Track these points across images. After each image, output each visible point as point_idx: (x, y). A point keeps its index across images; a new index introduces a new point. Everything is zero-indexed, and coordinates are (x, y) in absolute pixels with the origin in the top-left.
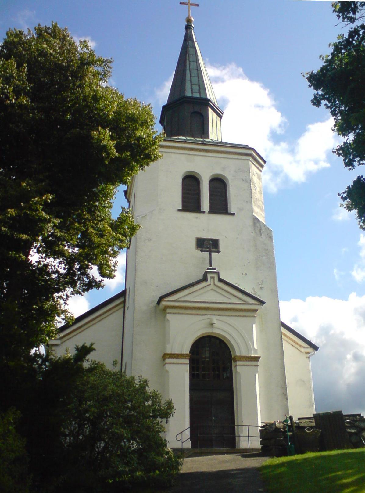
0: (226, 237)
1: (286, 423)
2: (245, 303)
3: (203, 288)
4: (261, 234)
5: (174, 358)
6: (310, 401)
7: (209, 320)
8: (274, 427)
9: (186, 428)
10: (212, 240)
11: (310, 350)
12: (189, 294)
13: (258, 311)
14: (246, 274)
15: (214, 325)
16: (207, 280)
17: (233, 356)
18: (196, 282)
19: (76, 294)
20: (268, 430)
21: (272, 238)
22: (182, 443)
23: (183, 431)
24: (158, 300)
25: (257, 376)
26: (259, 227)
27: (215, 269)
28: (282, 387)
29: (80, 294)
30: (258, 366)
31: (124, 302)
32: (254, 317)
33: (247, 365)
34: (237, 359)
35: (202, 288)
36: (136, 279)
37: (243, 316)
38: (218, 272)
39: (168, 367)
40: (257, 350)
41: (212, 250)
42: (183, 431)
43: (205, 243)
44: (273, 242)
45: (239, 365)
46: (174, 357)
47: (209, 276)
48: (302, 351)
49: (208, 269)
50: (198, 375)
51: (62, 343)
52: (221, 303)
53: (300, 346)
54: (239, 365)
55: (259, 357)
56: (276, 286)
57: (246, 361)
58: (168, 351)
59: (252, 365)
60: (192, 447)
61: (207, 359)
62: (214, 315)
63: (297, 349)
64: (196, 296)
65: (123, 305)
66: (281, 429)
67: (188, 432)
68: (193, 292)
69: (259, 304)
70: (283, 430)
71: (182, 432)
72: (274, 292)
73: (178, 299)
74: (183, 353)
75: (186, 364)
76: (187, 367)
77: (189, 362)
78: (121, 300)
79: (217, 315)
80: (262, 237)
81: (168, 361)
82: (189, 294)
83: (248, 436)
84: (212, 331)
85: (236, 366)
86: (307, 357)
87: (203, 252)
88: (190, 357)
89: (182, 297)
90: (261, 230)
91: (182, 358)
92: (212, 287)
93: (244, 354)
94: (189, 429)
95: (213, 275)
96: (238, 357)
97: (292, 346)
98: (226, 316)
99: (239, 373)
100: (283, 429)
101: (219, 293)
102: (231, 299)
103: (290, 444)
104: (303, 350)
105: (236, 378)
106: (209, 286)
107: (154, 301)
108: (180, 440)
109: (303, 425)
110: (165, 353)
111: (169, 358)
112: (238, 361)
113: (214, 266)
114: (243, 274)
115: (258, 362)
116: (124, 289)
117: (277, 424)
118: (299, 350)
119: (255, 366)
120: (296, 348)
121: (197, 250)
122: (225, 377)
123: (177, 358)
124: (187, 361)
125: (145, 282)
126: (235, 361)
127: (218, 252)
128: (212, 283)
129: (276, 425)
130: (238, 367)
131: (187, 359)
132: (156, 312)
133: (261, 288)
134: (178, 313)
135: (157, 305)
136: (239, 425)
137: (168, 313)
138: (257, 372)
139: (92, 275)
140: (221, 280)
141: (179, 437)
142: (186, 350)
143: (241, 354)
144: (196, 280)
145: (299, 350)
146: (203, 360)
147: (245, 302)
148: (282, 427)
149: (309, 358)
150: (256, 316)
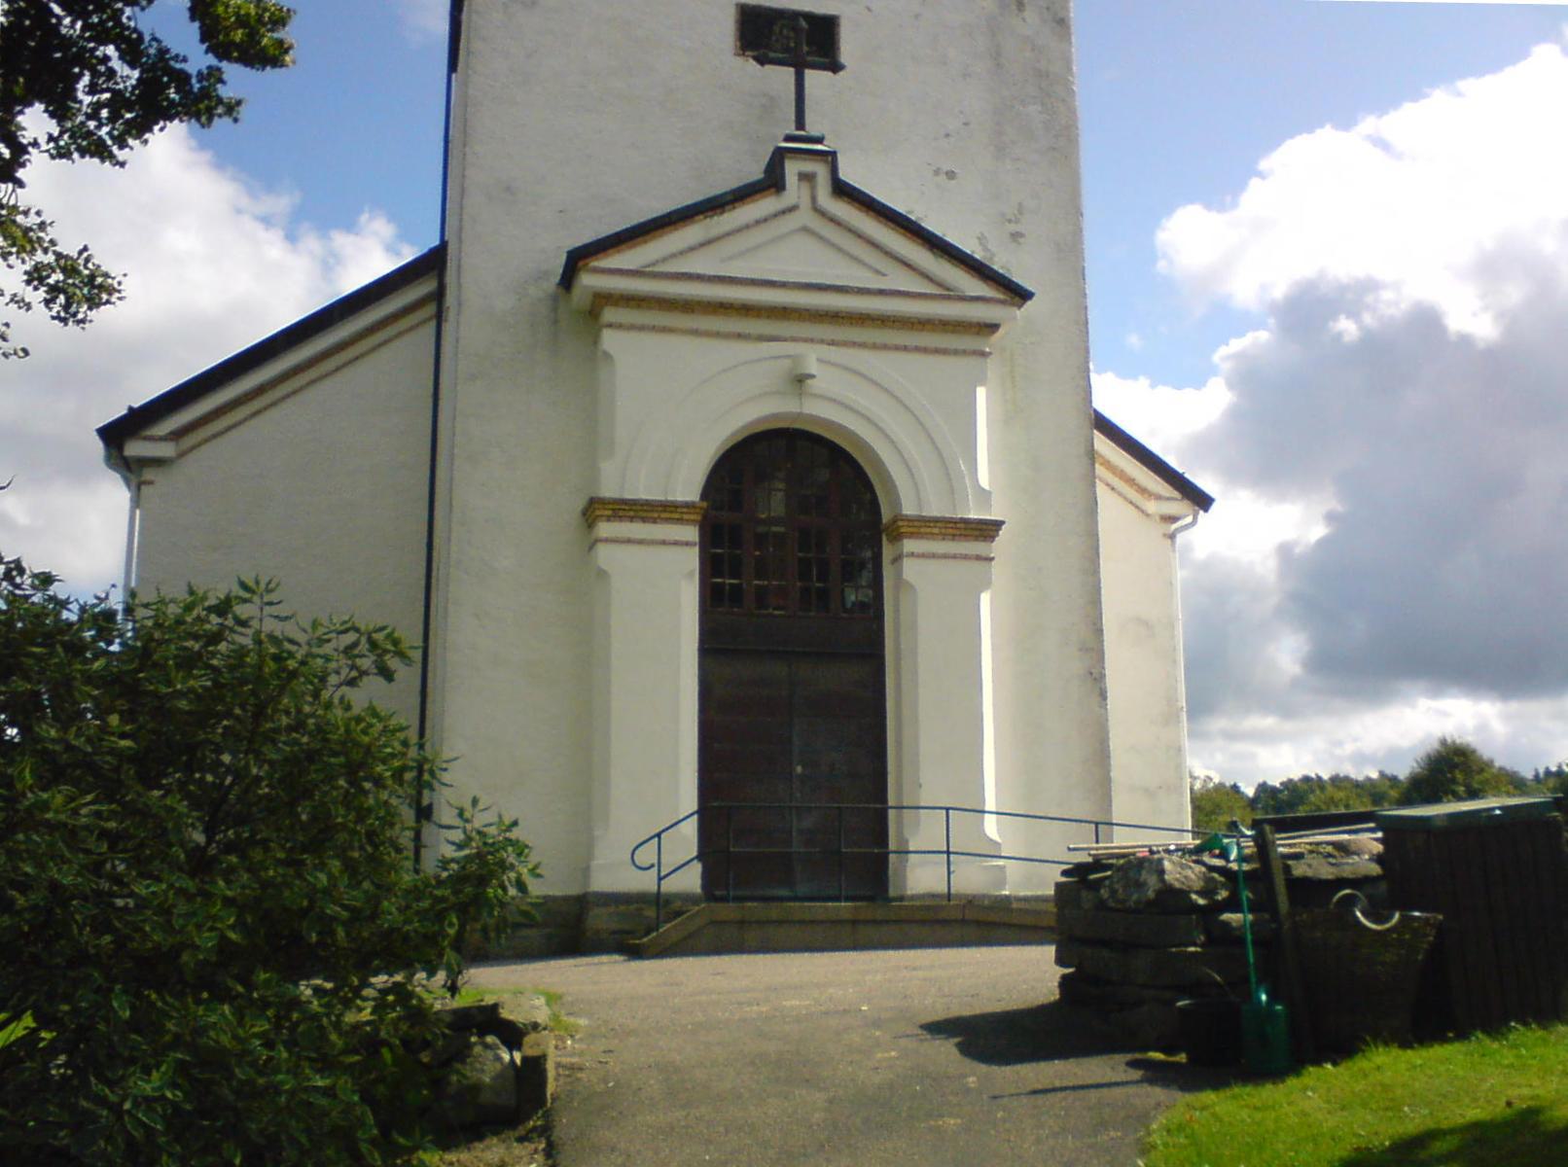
0: (869, 9)
1: (1218, 862)
2: (946, 293)
3: (765, 220)
5: (632, 519)
6: (1171, 701)
7: (787, 362)
8: (1152, 882)
9: (681, 817)
10: (809, 17)
11: (1180, 507)
12: (702, 245)
13: (1001, 331)
14: (951, 175)
15: (809, 382)
17: (886, 516)
18: (733, 192)
19: (83, 153)
20: (1113, 892)
21: (1068, 28)
22: (660, 879)
23: (663, 831)
24: (564, 272)
25: (985, 598)
27: (819, 140)
28: (1084, 649)
29: (100, 151)
30: (992, 559)
31: (439, 295)
32: (983, 354)
33: (945, 556)
35: (758, 222)
36: (467, 173)
37: (937, 351)
38: (833, 154)
39: (605, 555)
40: (990, 493)
41: (809, 58)
42: (663, 831)
43: (776, 29)
44: (1071, 43)
46: (632, 513)
47: (792, 168)
48: (1150, 512)
49: (789, 138)
50: (737, 591)
51: (182, 455)
53: (1143, 491)
54: (912, 555)
55: (998, 524)
56: (1078, 232)
57: (944, 537)
58: (609, 490)
59: (966, 557)
60: (704, 886)
61: (774, 529)
62: (812, 341)
63: (1131, 503)
64: (741, 254)
65: (430, 309)
66: (1194, 897)
67: (690, 829)
70: (1201, 901)
71: (658, 835)
72: (1070, 254)
73: (664, 260)
74: (670, 498)
76: (691, 559)
77: (697, 539)
78: (424, 287)
79: (822, 341)
80: (1024, 20)
81: (605, 529)
82: (702, 245)
83: (948, 853)
84: (799, 411)
85: (898, 559)
86: (1165, 535)
87: (769, 68)
88: (705, 517)
89: (673, 256)
91: (668, 520)
92: (805, 217)
93: (934, 509)
94: (696, 817)
95: (808, 166)
96: (910, 520)
97: (1110, 491)
98: (863, 345)
100: (1201, 893)
101: (833, 245)
102: (884, 275)
103: (1264, 997)
104: (1152, 507)
105: (897, 611)
106: (788, 216)
107: (545, 275)
108: (652, 866)
109: (1310, 873)
110: (594, 495)
111: (609, 519)
112: (911, 535)
113: (812, 128)
114: (937, 172)
115: (994, 544)
116: (436, 242)
117: (1167, 865)
118: (1137, 507)
119: (978, 558)
120: (1126, 499)
121: (740, 60)
122: (849, 605)
123: (644, 520)
124: (691, 533)
125: (508, 189)
126: (897, 537)
127: (835, 67)
129: (1162, 872)
130: (907, 563)
131: (688, 522)
132: (556, 322)
133: (1016, 236)
134: (654, 329)
135: (561, 291)
136: (905, 804)
137: (610, 326)
138: (986, 584)
139: (154, 39)
140: (843, 190)
141: (647, 855)
142: (688, 487)
143: (920, 506)
144: (734, 184)
145: (1137, 507)
146: (761, 529)
147: (948, 289)
148: (1198, 885)
149: (1172, 537)
150: (990, 353)
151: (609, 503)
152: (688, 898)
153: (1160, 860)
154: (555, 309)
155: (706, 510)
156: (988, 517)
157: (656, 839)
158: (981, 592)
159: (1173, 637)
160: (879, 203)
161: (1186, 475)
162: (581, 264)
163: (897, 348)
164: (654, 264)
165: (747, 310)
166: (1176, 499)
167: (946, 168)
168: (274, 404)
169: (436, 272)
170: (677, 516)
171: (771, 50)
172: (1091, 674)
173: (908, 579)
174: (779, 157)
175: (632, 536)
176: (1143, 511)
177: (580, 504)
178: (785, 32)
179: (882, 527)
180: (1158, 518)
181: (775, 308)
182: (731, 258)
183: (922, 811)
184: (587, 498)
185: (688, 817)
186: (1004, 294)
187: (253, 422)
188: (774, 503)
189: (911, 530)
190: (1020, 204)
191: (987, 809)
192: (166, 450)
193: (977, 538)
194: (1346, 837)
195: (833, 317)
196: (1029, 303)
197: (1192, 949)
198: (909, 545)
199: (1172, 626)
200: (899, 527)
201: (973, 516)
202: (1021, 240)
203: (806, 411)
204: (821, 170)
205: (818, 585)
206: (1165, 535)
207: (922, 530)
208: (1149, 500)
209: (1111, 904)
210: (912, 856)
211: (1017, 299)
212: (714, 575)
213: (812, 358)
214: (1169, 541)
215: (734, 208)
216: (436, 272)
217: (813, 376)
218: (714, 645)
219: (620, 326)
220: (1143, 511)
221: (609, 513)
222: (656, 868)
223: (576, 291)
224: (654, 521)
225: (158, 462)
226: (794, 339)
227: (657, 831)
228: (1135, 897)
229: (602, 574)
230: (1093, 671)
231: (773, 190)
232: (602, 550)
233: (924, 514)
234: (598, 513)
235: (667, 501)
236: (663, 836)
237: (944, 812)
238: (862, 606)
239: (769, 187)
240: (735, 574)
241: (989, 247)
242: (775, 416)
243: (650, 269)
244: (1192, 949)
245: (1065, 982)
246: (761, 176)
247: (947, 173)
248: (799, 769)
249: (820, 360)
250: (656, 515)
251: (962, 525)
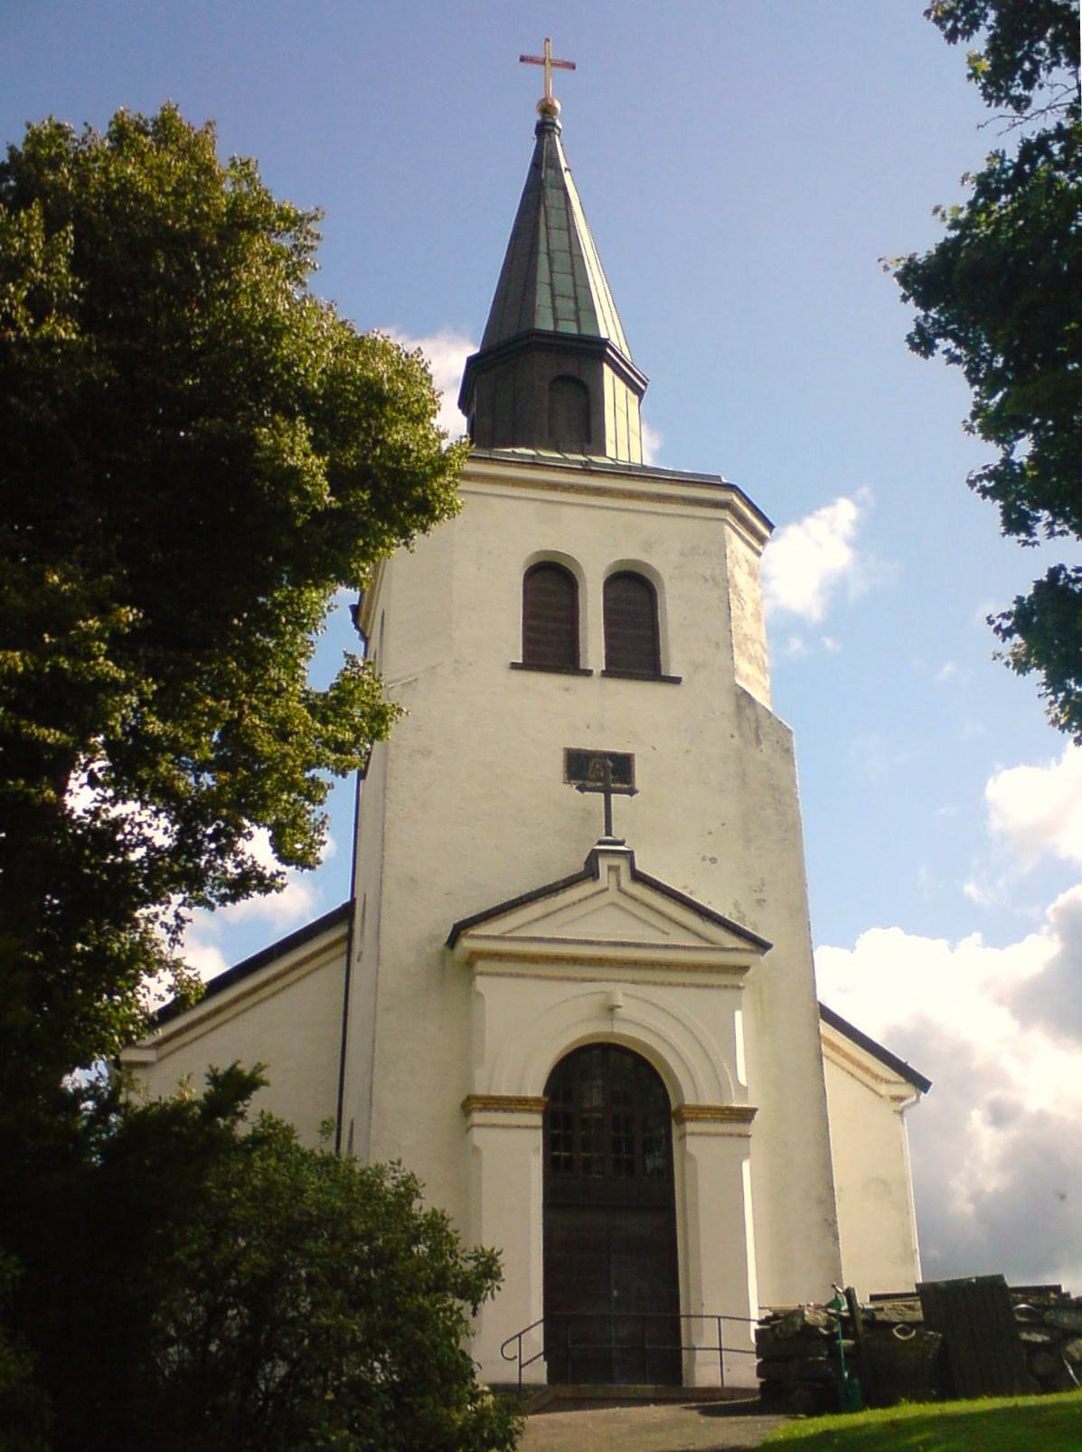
4: (759, 742)
5: (496, 1110)
6: (906, 1244)
8: (799, 1321)
11: (905, 1089)
12: (544, 917)
14: (713, 860)
17: (674, 1107)
18: (564, 881)
21: (792, 754)
22: (521, 1367)
23: (524, 1332)
27: (621, 843)
28: (821, 1202)
30: (750, 1136)
31: (349, 938)
32: (739, 988)
35: (580, 901)
37: (706, 986)
39: (478, 1136)
42: (524, 1332)
43: (591, 764)
45: (693, 1134)
47: (603, 864)
50: (568, 1162)
51: (160, 1059)
53: (876, 1077)
55: (753, 1111)
56: (804, 897)
57: (715, 1120)
58: (480, 1090)
61: (594, 1115)
65: (344, 946)
66: (821, 1330)
68: (555, 912)
69: (751, 951)
70: (825, 1332)
71: (519, 1335)
72: (799, 913)
73: (518, 928)
74: (523, 1095)
75: (535, 1127)
76: (537, 1138)
79: (626, 981)
81: (478, 1117)
82: (544, 917)
83: (720, 1349)
84: (610, 1030)
85: (682, 1137)
86: (895, 1111)
87: (587, 793)
89: (523, 925)
91: (520, 1111)
92: (612, 895)
93: (709, 1100)
94: (542, 1324)
95: (616, 861)
100: (826, 1328)
102: (667, 934)
104: (883, 1089)
108: (515, 1357)
109: (886, 1318)
110: (471, 1093)
111: (481, 1110)
112: (691, 1120)
113: (617, 834)
114: (704, 859)
117: (806, 1312)
118: (872, 1089)
119: (740, 1136)
120: (862, 1083)
122: (649, 1170)
123: (505, 1111)
124: (537, 1119)
126: (681, 1121)
127: (632, 792)
128: (613, 886)
130: (689, 1139)
133: (761, 902)
135: (448, 951)
137: (481, 974)
138: (747, 1155)
140: (638, 877)
141: (511, 1351)
142: (534, 1087)
145: (872, 1089)
146: (586, 1115)
147: (712, 943)
148: (823, 1323)
149: (901, 1113)
150: (743, 988)
152: (537, 1388)
154: (443, 961)
155: (547, 1104)
156: (745, 1106)
157: (518, 1339)
160: (663, 885)
161: (909, 1064)
162: (462, 932)
163: (678, 985)
167: (709, 856)
168: (226, 1021)
169: (347, 921)
171: (588, 779)
172: (826, 1220)
174: (594, 856)
175: (495, 1122)
177: (460, 1099)
178: (597, 766)
182: (563, 925)
185: (535, 1325)
187: (212, 1035)
188: (594, 1098)
189: (690, 1115)
190: (762, 879)
191: (752, 1318)
192: (149, 1056)
193: (737, 1121)
198: (691, 1127)
199: (904, 1184)
201: (735, 1105)
202: (765, 904)
203: (615, 1030)
204: (622, 864)
205: (626, 1156)
206: (895, 1111)
209: (782, 1336)
210: (698, 1352)
212: (553, 1150)
214: (899, 1117)
216: (347, 921)
217: (619, 1007)
218: (554, 1201)
222: (518, 1360)
224: (512, 1111)
225: (143, 1065)
229: (476, 1150)
233: (701, 1103)
236: (523, 1336)
239: (589, 876)
240: (568, 1148)
242: (597, 1035)
243: (510, 935)
245: (762, 1384)
246: (583, 869)
247: (711, 860)
249: (625, 995)
251: (727, 1112)
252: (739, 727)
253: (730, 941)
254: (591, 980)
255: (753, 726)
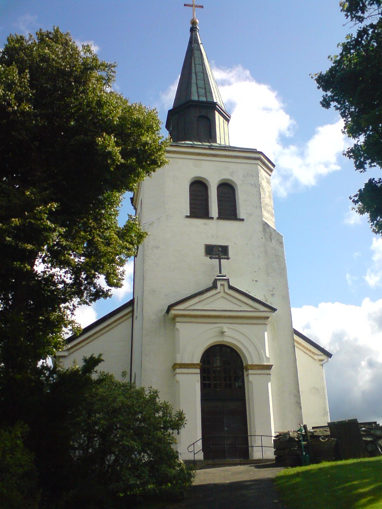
2: (256, 310)
4: (271, 240)
6: (325, 410)
7: (220, 328)
8: (288, 436)
9: (198, 440)
10: (221, 246)
11: (324, 357)
14: (256, 281)
16: (217, 288)
18: (205, 290)
20: (282, 439)
21: (283, 244)
25: (270, 384)
26: (269, 232)
27: (225, 276)
28: (295, 396)
29: (87, 304)
30: (270, 374)
31: (133, 311)
34: (248, 368)
35: (211, 296)
36: (144, 287)
38: (228, 279)
39: (178, 377)
43: (214, 249)
47: (219, 283)
49: (218, 276)
50: (209, 384)
51: (70, 354)
52: (231, 311)
53: (313, 353)
55: (272, 366)
56: (288, 293)
58: (179, 361)
59: (264, 374)
63: (310, 356)
65: (131, 314)
66: (295, 439)
67: (200, 443)
68: (202, 300)
69: (270, 312)
70: (297, 440)
71: (194, 444)
72: (286, 298)
73: (190, 306)
74: (193, 363)
77: (199, 372)
78: (129, 310)
79: (227, 323)
81: (178, 371)
83: (262, 446)
85: (248, 375)
86: (320, 365)
88: (201, 367)
90: (271, 235)
91: (193, 368)
92: (222, 294)
93: (256, 362)
94: (201, 440)
95: (223, 282)
96: (250, 365)
99: (251, 382)
100: (297, 438)
101: (229, 300)
104: (316, 357)
107: (162, 310)
108: (192, 451)
109: (317, 434)
110: (175, 363)
111: (179, 368)
112: (250, 369)
114: (253, 281)
115: (271, 371)
116: (132, 298)
117: (290, 433)
119: (267, 374)
120: (309, 355)
121: (206, 257)
123: (187, 368)
124: (198, 371)
125: (154, 291)
126: (247, 370)
127: (228, 259)
128: (222, 291)
129: (290, 434)
130: (250, 376)
131: (198, 368)
133: (272, 295)
136: (252, 435)
137: (178, 322)
138: (270, 380)
140: (231, 288)
141: (191, 449)
142: (197, 360)
143: (252, 362)
146: (214, 369)
147: (257, 309)
148: (296, 437)
149: (322, 365)
150: (268, 324)
151: (179, 364)
152: (200, 461)
153: (289, 433)
157: (193, 445)
158: (269, 382)
159: (324, 392)
162: (171, 308)
163: (245, 324)
164: (188, 307)
165: (209, 317)
166: (322, 355)
170: (195, 367)
173: (251, 380)
174: (215, 281)
176: (314, 359)
179: (244, 367)
180: (318, 360)
181: (216, 316)
183: (256, 436)
184: (174, 363)
186: (270, 310)
189: (250, 368)
192: (65, 354)
194: (326, 429)
195: (230, 317)
196: (276, 312)
197: (296, 448)
200: (248, 367)
206: (320, 365)
207: (253, 368)
208: (315, 356)
211: (273, 311)
213: (225, 328)
215: (206, 293)
216: (132, 306)
219: (180, 322)
220: (314, 359)
221: (179, 367)
223: (170, 314)
226: (221, 323)
227: (193, 443)
228: (285, 439)
230: (298, 402)
231: (214, 289)
232: (177, 376)
234: (176, 367)
235: (192, 363)
237: (260, 436)
238: (239, 387)
241: (266, 298)
244: (296, 448)
248: (226, 429)
250: (190, 367)
252: (264, 235)
253: (262, 308)
254: (216, 323)
255: (269, 234)
